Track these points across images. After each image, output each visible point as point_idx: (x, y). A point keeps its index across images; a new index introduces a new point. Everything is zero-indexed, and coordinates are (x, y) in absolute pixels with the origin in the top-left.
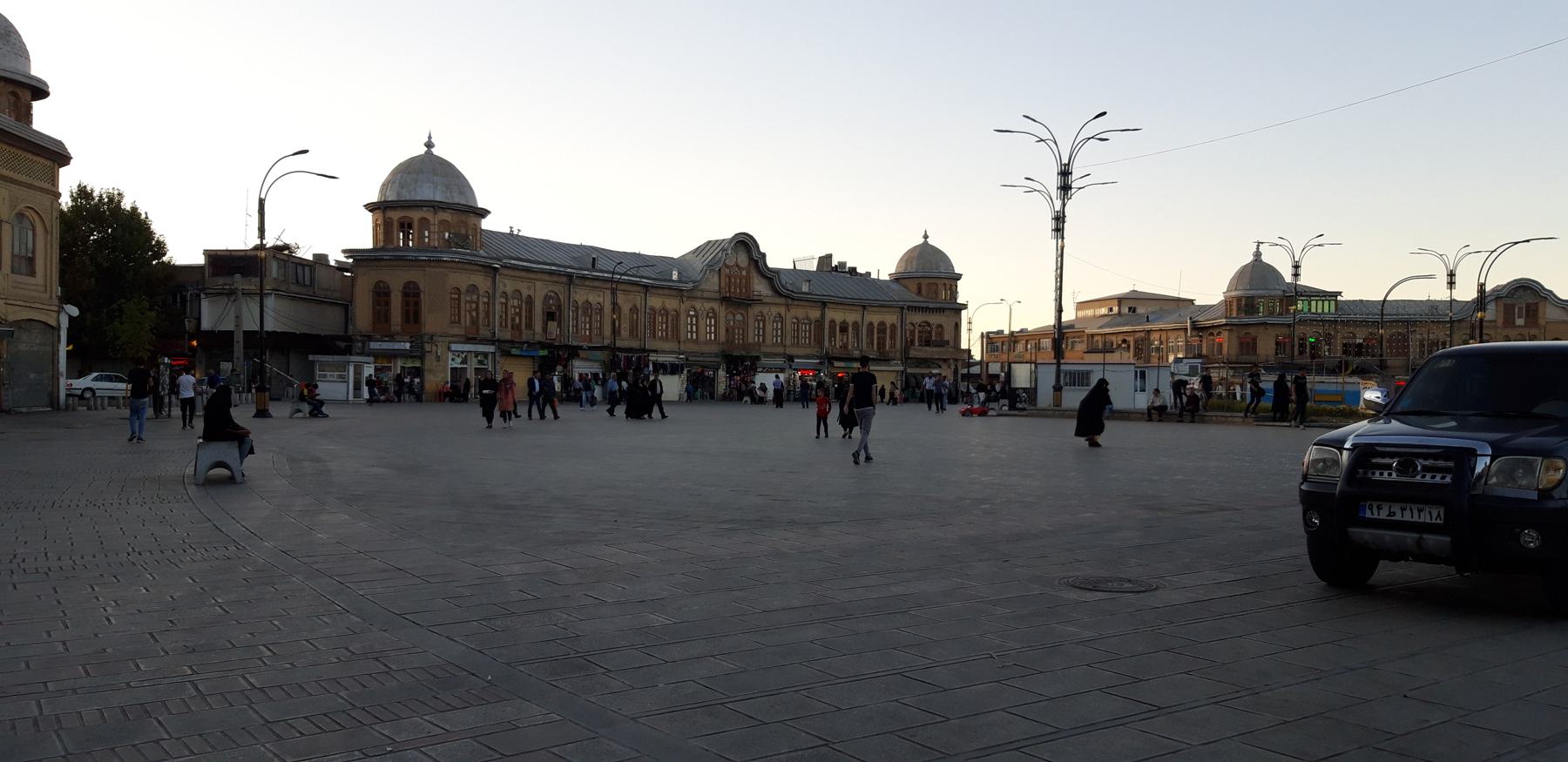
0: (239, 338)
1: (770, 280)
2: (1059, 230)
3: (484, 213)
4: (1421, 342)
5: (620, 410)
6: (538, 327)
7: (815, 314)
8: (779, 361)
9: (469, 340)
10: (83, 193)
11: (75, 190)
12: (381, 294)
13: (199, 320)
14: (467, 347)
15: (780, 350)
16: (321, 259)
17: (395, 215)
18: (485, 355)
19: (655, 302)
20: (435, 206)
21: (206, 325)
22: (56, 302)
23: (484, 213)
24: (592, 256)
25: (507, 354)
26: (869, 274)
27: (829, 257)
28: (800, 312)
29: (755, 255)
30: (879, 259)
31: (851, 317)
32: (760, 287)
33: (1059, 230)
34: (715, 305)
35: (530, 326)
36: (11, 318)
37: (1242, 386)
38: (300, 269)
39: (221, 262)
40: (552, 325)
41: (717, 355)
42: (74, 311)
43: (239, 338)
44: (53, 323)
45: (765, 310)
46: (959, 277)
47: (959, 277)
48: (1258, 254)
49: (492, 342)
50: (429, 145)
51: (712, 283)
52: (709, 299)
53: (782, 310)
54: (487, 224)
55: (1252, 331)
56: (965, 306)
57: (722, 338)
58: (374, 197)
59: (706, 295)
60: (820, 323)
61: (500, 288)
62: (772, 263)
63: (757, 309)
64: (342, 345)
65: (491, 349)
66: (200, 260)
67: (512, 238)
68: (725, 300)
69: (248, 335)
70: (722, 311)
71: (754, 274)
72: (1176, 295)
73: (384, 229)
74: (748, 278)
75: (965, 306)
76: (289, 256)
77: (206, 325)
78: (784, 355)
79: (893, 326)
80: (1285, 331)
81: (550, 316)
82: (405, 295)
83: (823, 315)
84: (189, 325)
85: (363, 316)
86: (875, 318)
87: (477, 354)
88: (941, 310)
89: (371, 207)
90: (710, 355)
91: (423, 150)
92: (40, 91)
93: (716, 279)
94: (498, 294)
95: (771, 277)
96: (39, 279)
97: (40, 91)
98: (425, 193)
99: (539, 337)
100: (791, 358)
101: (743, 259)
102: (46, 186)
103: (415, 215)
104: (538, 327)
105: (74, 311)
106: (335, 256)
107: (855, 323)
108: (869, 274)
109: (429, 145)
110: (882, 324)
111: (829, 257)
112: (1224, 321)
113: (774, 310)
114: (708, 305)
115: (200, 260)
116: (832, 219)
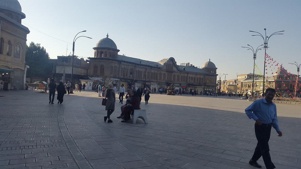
0: (64, 75)
1: (177, 68)
2: (255, 58)
3: (119, 51)
6: (128, 75)
7: (186, 75)
8: (178, 85)
10: (32, 44)
11: (31, 43)
12: (95, 67)
13: (56, 71)
15: (178, 82)
16: (82, 59)
18: (117, 81)
20: (109, 49)
21: (57, 72)
22: (24, 64)
23: (119, 51)
24: (141, 61)
25: (121, 81)
26: (197, 67)
27: (189, 63)
28: (183, 75)
30: (201, 65)
31: (194, 76)
32: (175, 69)
33: (255, 58)
34: (165, 72)
35: (127, 75)
36: (13, 68)
37: (122, 95)
38: (78, 61)
39: (62, 59)
40: (131, 76)
42: (28, 67)
44: (23, 69)
46: (217, 68)
47: (217, 68)
49: (119, 78)
50: (108, 36)
52: (164, 71)
54: (119, 53)
56: (218, 75)
58: (95, 46)
59: (163, 70)
63: (174, 73)
64: (86, 77)
66: (57, 58)
67: (123, 56)
68: (168, 71)
72: (54, 98)
73: (97, 54)
75: (218, 75)
76: (76, 58)
77: (57, 72)
78: (179, 84)
79: (202, 79)
81: (131, 73)
83: (188, 75)
84: (53, 72)
85: (91, 71)
86: (199, 77)
87: (116, 81)
88: (213, 75)
89: (95, 48)
92: (24, 16)
94: (121, 68)
95: (178, 67)
97: (24, 16)
98: (107, 46)
100: (180, 84)
101: (171, 63)
105: (28, 67)
106: (85, 59)
107: (194, 77)
108: (197, 67)
109: (108, 36)
110: (200, 78)
111: (189, 63)
112: (274, 80)
113: (177, 74)
114: (164, 72)
115: (57, 58)
116: (191, 56)
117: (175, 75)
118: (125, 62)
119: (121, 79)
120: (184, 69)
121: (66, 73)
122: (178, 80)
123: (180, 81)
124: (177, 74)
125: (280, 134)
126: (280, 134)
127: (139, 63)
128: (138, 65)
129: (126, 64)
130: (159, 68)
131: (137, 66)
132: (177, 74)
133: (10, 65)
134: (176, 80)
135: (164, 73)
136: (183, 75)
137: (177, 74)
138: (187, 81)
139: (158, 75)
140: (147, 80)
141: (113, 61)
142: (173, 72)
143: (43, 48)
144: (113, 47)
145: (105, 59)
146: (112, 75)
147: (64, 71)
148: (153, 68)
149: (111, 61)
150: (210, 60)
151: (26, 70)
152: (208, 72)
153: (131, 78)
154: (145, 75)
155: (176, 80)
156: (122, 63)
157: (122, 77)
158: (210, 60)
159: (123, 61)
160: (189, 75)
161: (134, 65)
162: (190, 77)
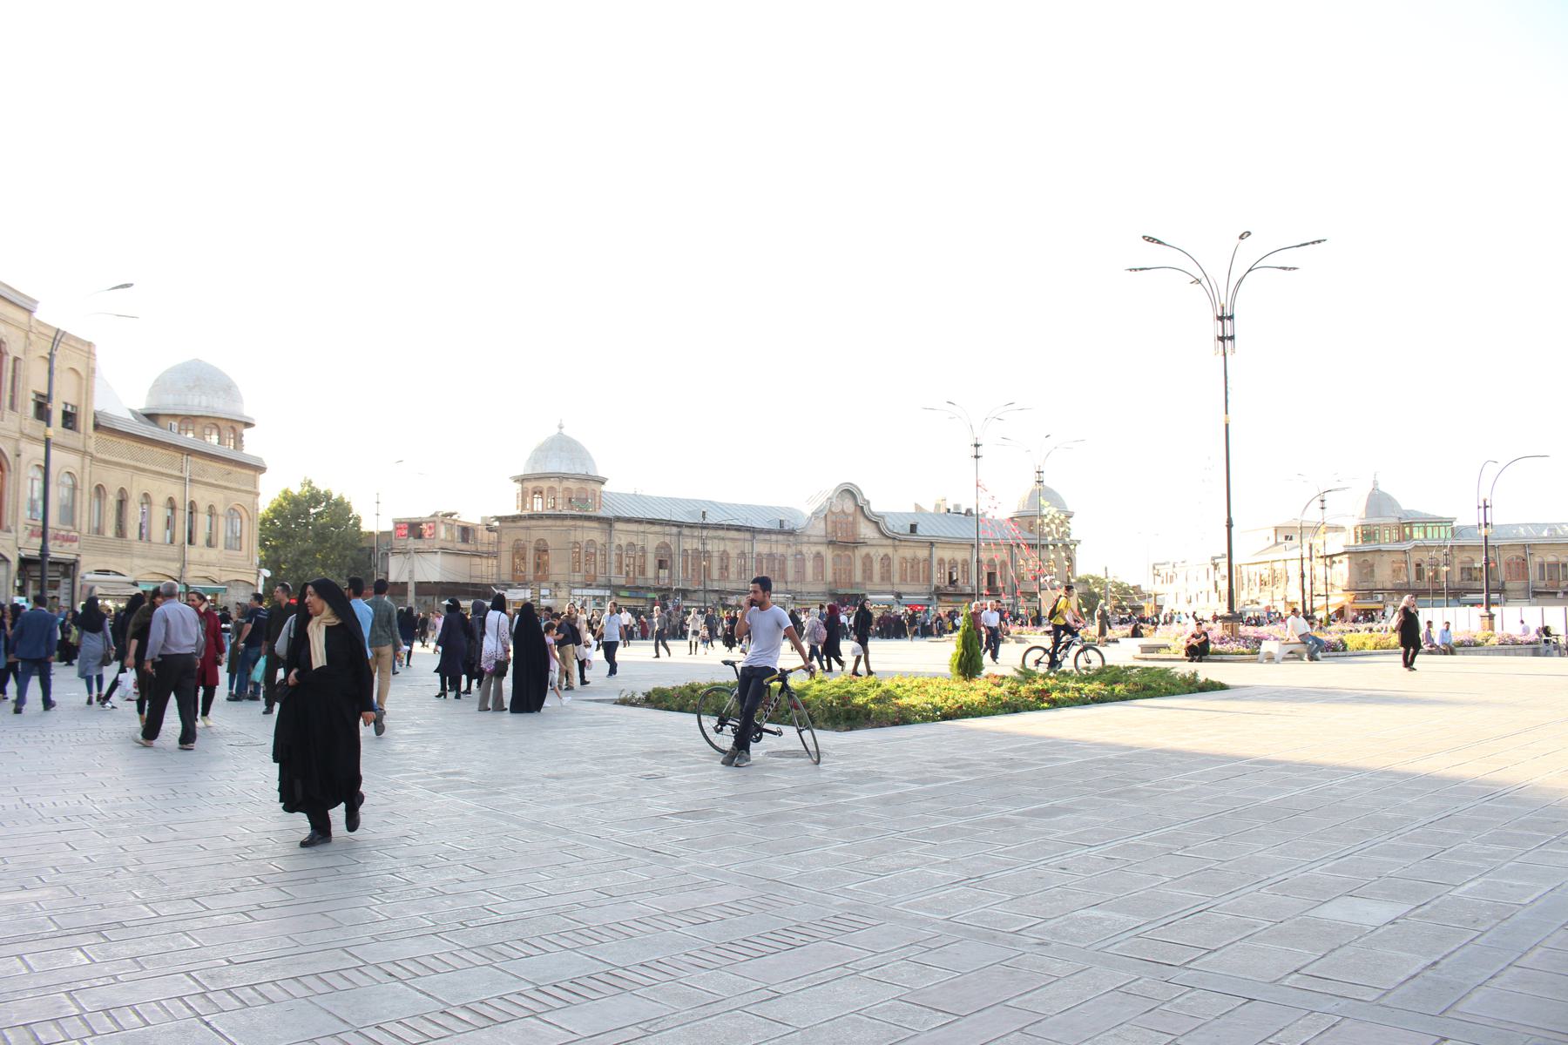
0: (411, 588)
4: (1542, 566)
5: (1194, 642)
6: (650, 573)
7: (922, 553)
9: (588, 586)
14: (585, 592)
15: (888, 588)
17: (530, 485)
18: (603, 598)
19: (761, 547)
21: (392, 578)
28: (908, 553)
29: (860, 502)
32: (866, 531)
34: (823, 549)
36: (224, 580)
40: (664, 573)
41: (824, 594)
42: (267, 573)
43: (411, 588)
45: (872, 551)
48: (1375, 483)
51: (819, 529)
53: (890, 551)
55: (1369, 557)
57: (829, 576)
60: (929, 560)
61: (617, 541)
62: (876, 507)
63: (863, 551)
65: (608, 593)
69: (419, 585)
70: (828, 553)
71: (861, 519)
74: (854, 524)
77: (392, 578)
79: (1003, 564)
80: (1401, 557)
81: (661, 564)
82: (537, 549)
87: (595, 597)
90: (817, 594)
91: (557, 430)
93: (822, 525)
94: (614, 546)
95: (876, 522)
96: (244, 552)
99: (652, 583)
101: (849, 506)
102: (249, 488)
103: (544, 485)
104: (650, 573)
105: (267, 573)
114: (814, 549)
117: (868, 556)
118: (629, 520)
119: (616, 589)
120: (913, 528)
121: (421, 577)
122: (887, 576)
123: (896, 579)
124: (877, 553)
125: (48, 703)
126: (48, 703)
127: (701, 520)
128: (691, 526)
129: (633, 527)
130: (791, 533)
131: (686, 531)
132: (877, 553)
133: (214, 573)
134: (876, 578)
135: (818, 555)
136: (908, 553)
137: (882, 551)
138: (929, 579)
139: (790, 563)
140: (730, 586)
141: (579, 523)
142: (856, 544)
143: (341, 498)
144: (579, 470)
145: (549, 517)
146: (578, 578)
147: (411, 572)
148: (762, 537)
149: (572, 523)
150: (561, 427)
151: (261, 582)
152: (1031, 531)
153: (664, 583)
154: (724, 568)
155: (876, 578)
156: (618, 526)
157: (622, 581)
158: (561, 427)
159: (618, 519)
160: (938, 553)
161: (675, 530)
162: (941, 562)
